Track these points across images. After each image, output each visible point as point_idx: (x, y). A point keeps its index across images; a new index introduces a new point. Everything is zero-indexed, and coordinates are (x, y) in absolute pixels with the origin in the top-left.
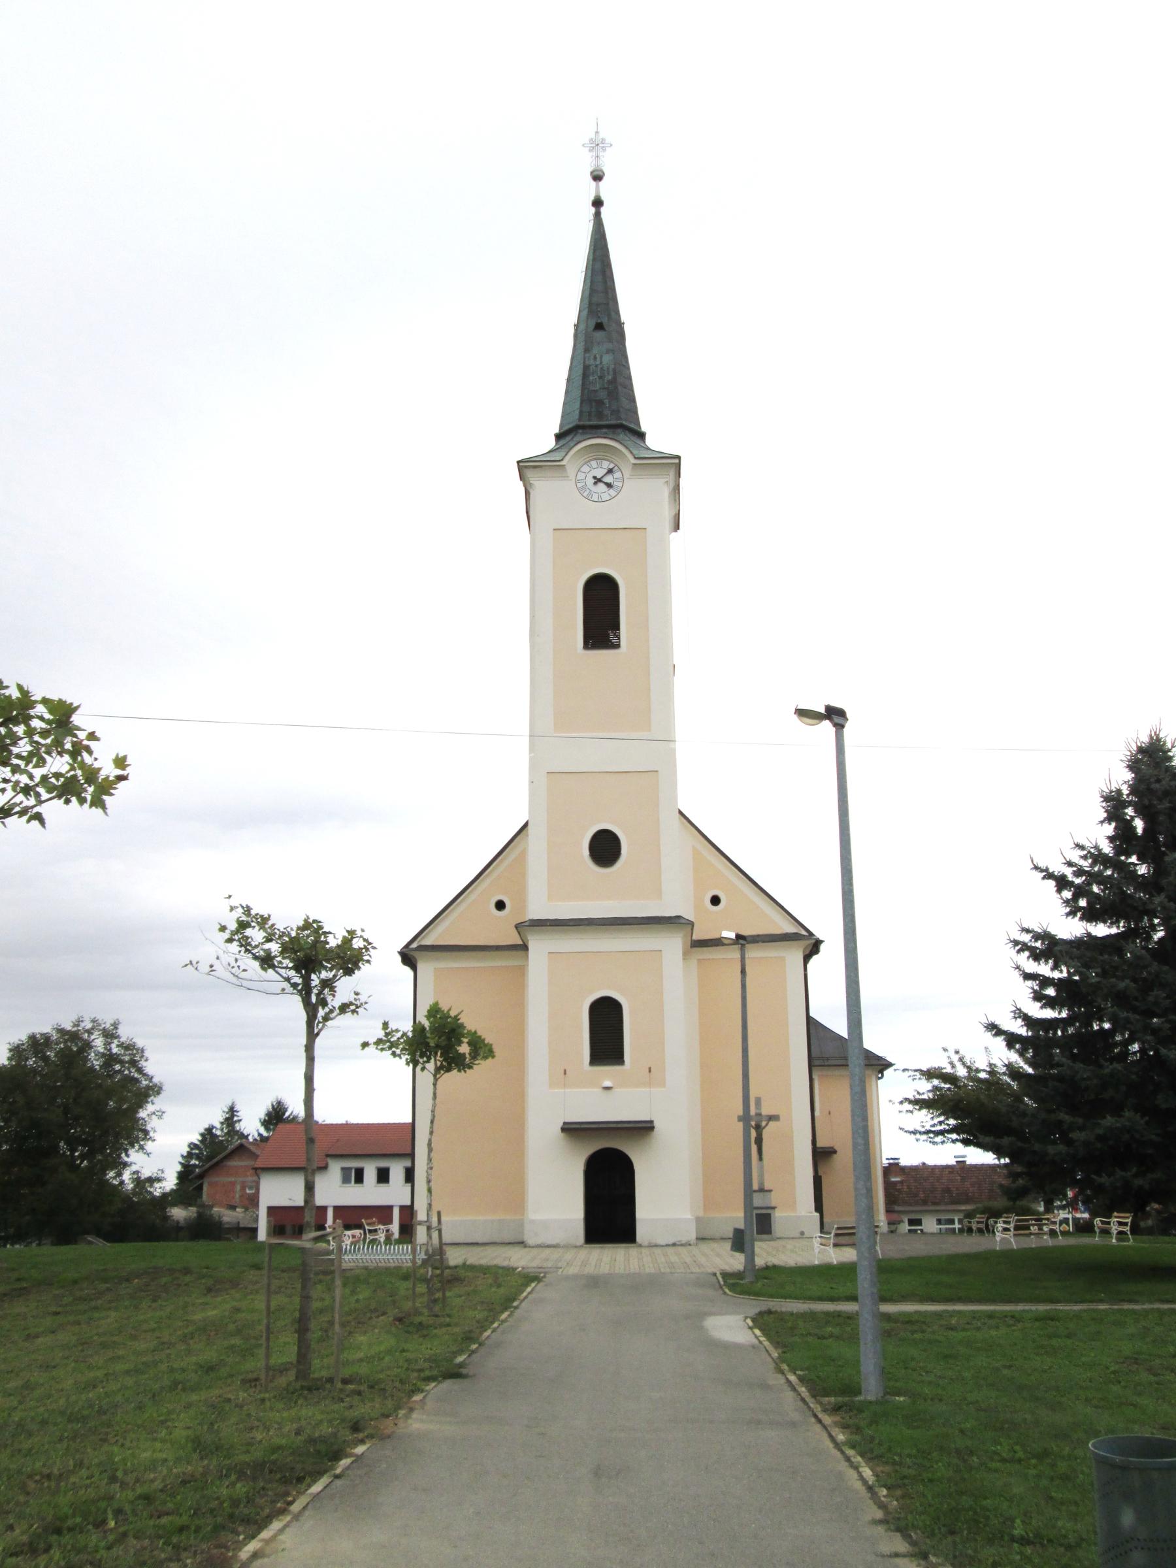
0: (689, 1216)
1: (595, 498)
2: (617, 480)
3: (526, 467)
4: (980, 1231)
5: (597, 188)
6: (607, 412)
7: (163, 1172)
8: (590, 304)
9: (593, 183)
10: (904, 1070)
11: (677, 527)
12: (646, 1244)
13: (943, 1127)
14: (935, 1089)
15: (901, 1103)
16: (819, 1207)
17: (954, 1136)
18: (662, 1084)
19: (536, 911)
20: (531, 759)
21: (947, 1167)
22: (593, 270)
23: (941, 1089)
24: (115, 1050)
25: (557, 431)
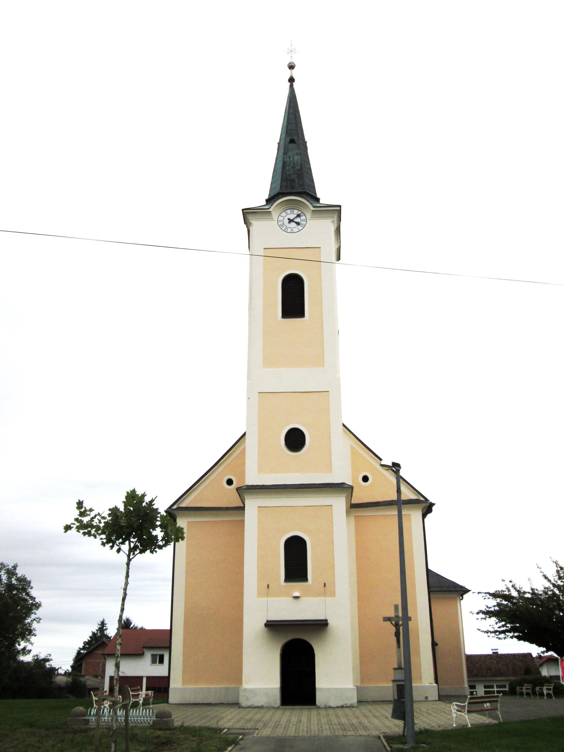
0: (353, 687)
1: (289, 230)
2: (303, 220)
3: (248, 214)
4: (528, 694)
5: (291, 72)
6: (297, 186)
7: (50, 655)
8: (287, 130)
9: (290, 71)
10: (479, 593)
11: (339, 258)
12: (323, 706)
13: (504, 628)
14: (499, 605)
15: (478, 613)
16: (436, 681)
17: (511, 634)
18: (333, 594)
19: (251, 480)
20: (248, 384)
21: (488, 655)
22: (289, 113)
23: (502, 604)
24: (14, 582)
25: (267, 197)
